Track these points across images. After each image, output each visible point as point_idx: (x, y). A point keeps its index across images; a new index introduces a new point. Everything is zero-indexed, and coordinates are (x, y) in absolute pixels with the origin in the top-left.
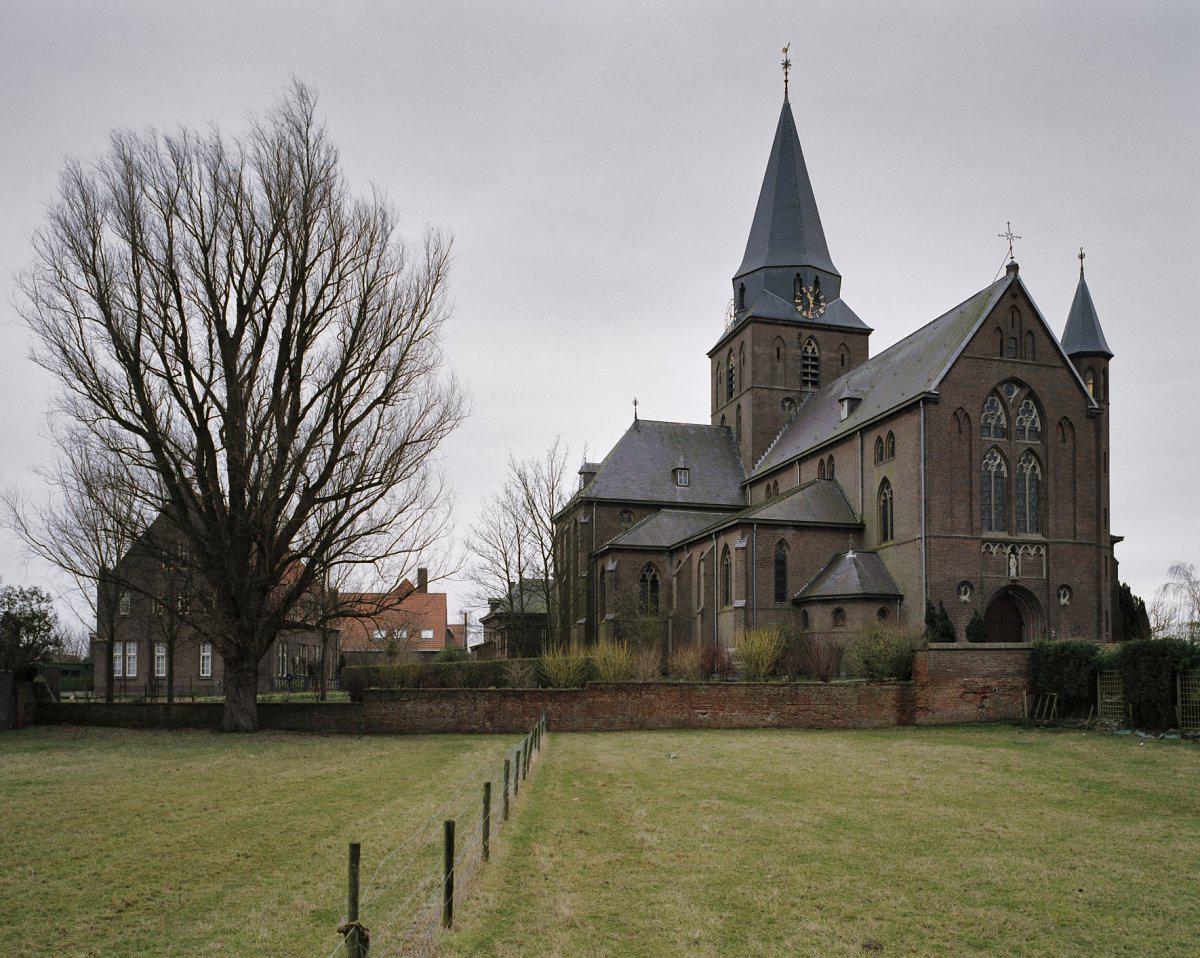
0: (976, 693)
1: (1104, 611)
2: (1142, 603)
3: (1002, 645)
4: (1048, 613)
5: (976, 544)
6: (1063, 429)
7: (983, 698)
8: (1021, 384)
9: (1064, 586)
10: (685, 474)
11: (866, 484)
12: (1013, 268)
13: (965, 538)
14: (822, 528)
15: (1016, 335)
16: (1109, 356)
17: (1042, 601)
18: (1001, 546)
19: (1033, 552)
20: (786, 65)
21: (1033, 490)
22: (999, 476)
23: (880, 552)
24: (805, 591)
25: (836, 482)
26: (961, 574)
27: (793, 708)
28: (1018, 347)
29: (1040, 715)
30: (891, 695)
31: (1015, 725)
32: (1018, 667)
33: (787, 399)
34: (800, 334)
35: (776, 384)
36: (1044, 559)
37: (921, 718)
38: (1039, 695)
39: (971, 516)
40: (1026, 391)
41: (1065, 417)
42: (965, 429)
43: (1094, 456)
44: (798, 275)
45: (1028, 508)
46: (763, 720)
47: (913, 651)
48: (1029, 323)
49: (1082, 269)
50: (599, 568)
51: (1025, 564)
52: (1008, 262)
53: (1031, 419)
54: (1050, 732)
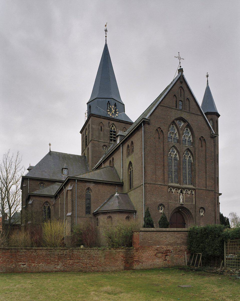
0: (162, 253)
1: (217, 219)
2: (228, 219)
3: (175, 229)
4: (195, 219)
5: (166, 187)
6: (201, 142)
7: (167, 255)
8: (184, 121)
9: (202, 208)
10: (66, 171)
11: (124, 166)
12: (181, 70)
13: (161, 185)
14: (106, 183)
15: (182, 100)
16: (218, 116)
17: (193, 214)
18: (176, 190)
19: (189, 192)
20: (106, 31)
21: (189, 167)
22: (175, 159)
23: (129, 194)
24: (99, 209)
25: (114, 168)
26: (160, 201)
27: (71, 261)
28: (183, 105)
29: (193, 264)
30: (121, 254)
31: (181, 269)
32: (183, 240)
33: (105, 146)
34: (109, 123)
35: (100, 140)
36: (194, 196)
37: (136, 266)
38: (193, 254)
39: (164, 176)
40: (187, 124)
41: (202, 137)
42: (161, 137)
43: (213, 154)
44: (109, 102)
45: (187, 175)
46: (55, 268)
47: (132, 232)
48: (187, 95)
49: (208, 81)
51: (186, 198)
52: (179, 68)
53: (188, 136)
54: (199, 274)
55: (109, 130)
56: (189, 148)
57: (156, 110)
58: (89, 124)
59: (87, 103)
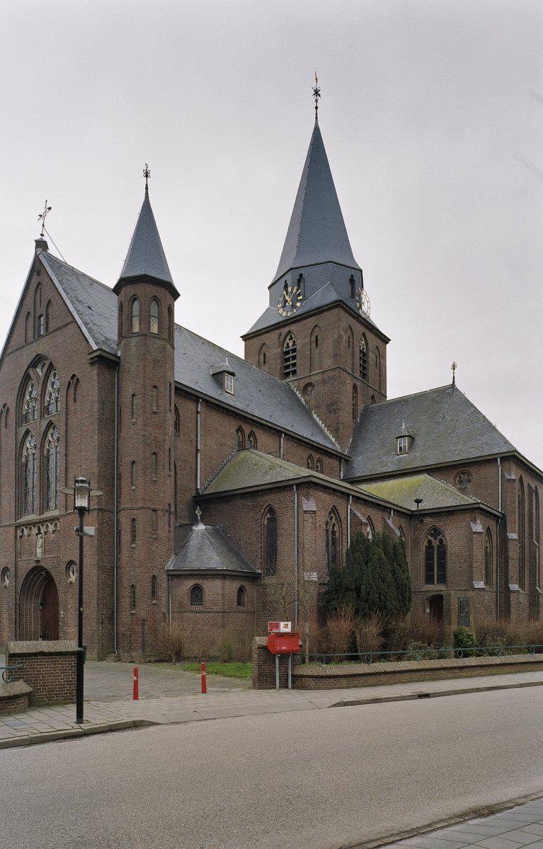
12: (41, 245)
20: (317, 93)
34: (280, 334)
49: (147, 188)
50: (494, 538)
52: (39, 237)
58: (50, 301)
59: (269, 288)
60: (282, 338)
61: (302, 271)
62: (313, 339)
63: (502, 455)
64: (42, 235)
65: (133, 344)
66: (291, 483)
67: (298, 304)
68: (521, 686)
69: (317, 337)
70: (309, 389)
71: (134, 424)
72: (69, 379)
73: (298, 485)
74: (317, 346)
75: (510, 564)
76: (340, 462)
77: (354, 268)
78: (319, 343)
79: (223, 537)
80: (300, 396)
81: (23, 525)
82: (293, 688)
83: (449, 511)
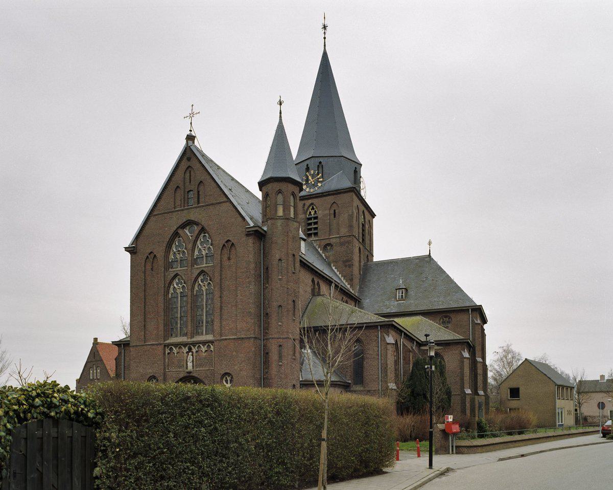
5: (161, 348)
12: (190, 138)
20: (325, 27)
34: (304, 205)
49: (281, 113)
55: (304, 219)
56: (204, 269)
57: (147, 227)
60: (306, 207)
61: (321, 160)
62: (332, 212)
63: (473, 307)
64: (191, 131)
65: (279, 224)
66: (378, 324)
67: (319, 185)
68: (551, 450)
69: (335, 211)
70: (329, 248)
71: (280, 280)
72: (224, 242)
73: (381, 326)
74: (335, 217)
75: (478, 378)
76: (356, 303)
77: (354, 162)
78: (336, 216)
79: (322, 356)
80: (321, 252)
81: (181, 345)
82: (457, 453)
83: (447, 343)
